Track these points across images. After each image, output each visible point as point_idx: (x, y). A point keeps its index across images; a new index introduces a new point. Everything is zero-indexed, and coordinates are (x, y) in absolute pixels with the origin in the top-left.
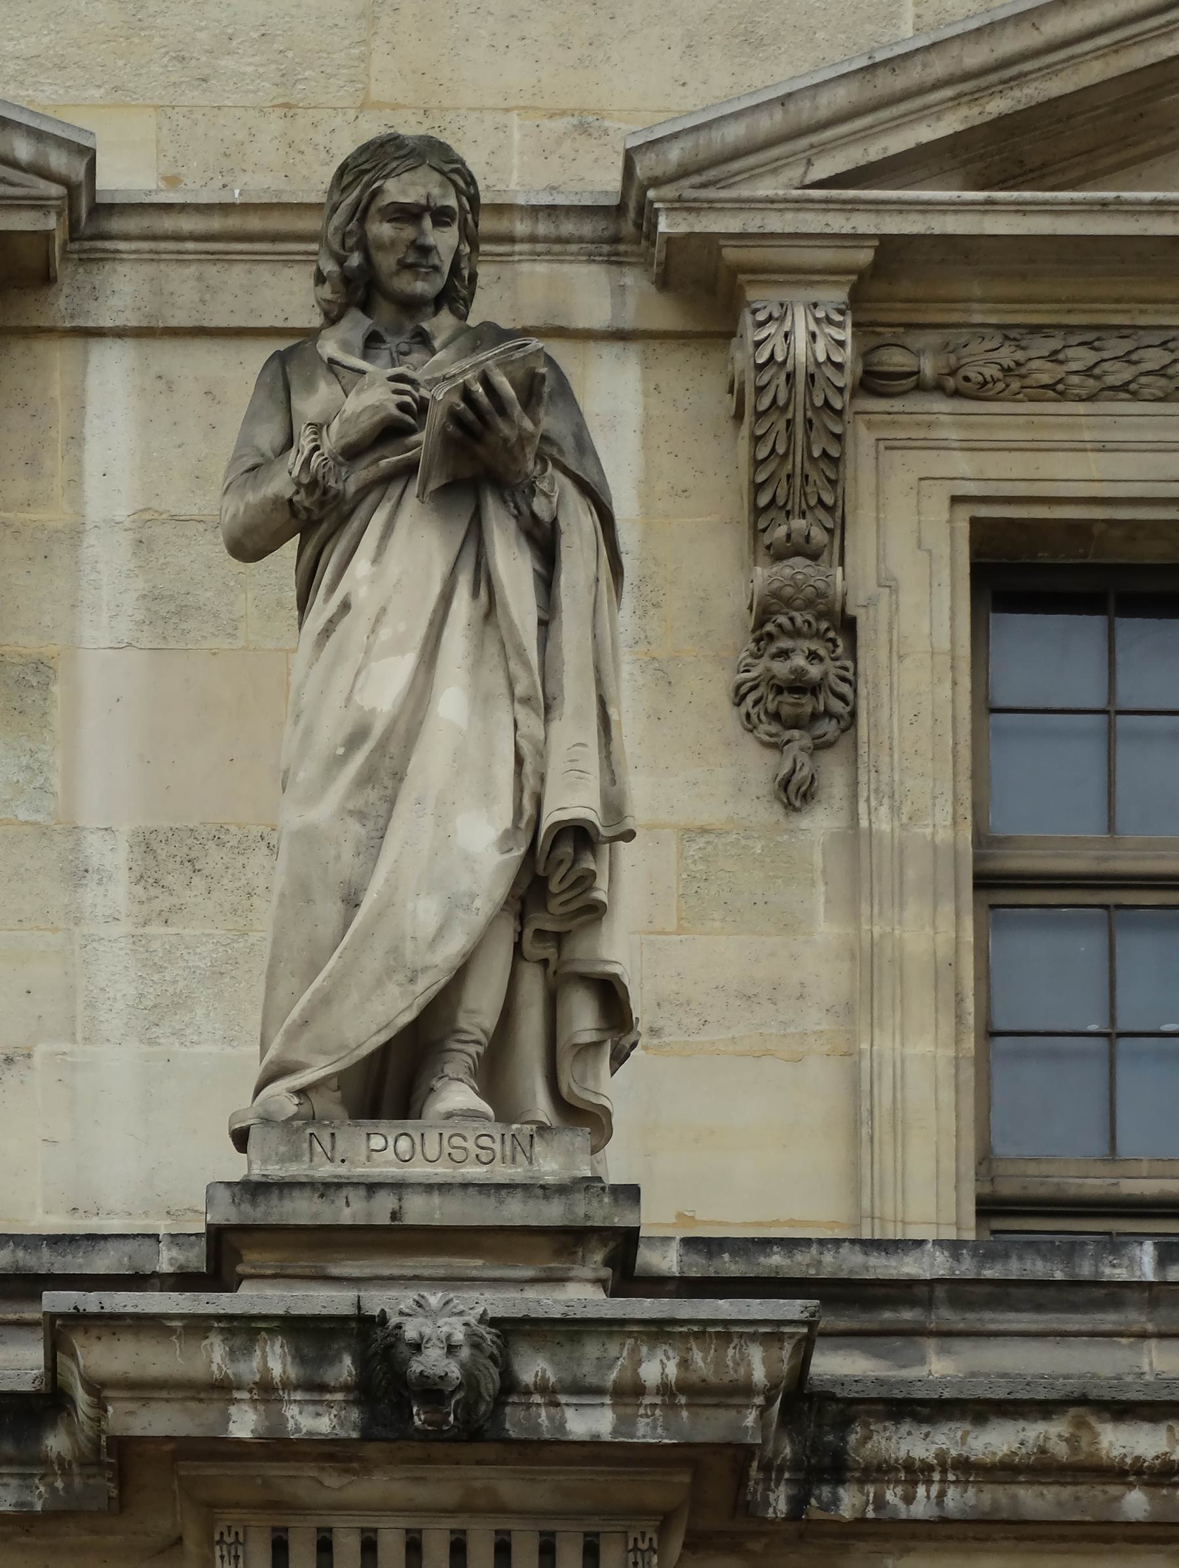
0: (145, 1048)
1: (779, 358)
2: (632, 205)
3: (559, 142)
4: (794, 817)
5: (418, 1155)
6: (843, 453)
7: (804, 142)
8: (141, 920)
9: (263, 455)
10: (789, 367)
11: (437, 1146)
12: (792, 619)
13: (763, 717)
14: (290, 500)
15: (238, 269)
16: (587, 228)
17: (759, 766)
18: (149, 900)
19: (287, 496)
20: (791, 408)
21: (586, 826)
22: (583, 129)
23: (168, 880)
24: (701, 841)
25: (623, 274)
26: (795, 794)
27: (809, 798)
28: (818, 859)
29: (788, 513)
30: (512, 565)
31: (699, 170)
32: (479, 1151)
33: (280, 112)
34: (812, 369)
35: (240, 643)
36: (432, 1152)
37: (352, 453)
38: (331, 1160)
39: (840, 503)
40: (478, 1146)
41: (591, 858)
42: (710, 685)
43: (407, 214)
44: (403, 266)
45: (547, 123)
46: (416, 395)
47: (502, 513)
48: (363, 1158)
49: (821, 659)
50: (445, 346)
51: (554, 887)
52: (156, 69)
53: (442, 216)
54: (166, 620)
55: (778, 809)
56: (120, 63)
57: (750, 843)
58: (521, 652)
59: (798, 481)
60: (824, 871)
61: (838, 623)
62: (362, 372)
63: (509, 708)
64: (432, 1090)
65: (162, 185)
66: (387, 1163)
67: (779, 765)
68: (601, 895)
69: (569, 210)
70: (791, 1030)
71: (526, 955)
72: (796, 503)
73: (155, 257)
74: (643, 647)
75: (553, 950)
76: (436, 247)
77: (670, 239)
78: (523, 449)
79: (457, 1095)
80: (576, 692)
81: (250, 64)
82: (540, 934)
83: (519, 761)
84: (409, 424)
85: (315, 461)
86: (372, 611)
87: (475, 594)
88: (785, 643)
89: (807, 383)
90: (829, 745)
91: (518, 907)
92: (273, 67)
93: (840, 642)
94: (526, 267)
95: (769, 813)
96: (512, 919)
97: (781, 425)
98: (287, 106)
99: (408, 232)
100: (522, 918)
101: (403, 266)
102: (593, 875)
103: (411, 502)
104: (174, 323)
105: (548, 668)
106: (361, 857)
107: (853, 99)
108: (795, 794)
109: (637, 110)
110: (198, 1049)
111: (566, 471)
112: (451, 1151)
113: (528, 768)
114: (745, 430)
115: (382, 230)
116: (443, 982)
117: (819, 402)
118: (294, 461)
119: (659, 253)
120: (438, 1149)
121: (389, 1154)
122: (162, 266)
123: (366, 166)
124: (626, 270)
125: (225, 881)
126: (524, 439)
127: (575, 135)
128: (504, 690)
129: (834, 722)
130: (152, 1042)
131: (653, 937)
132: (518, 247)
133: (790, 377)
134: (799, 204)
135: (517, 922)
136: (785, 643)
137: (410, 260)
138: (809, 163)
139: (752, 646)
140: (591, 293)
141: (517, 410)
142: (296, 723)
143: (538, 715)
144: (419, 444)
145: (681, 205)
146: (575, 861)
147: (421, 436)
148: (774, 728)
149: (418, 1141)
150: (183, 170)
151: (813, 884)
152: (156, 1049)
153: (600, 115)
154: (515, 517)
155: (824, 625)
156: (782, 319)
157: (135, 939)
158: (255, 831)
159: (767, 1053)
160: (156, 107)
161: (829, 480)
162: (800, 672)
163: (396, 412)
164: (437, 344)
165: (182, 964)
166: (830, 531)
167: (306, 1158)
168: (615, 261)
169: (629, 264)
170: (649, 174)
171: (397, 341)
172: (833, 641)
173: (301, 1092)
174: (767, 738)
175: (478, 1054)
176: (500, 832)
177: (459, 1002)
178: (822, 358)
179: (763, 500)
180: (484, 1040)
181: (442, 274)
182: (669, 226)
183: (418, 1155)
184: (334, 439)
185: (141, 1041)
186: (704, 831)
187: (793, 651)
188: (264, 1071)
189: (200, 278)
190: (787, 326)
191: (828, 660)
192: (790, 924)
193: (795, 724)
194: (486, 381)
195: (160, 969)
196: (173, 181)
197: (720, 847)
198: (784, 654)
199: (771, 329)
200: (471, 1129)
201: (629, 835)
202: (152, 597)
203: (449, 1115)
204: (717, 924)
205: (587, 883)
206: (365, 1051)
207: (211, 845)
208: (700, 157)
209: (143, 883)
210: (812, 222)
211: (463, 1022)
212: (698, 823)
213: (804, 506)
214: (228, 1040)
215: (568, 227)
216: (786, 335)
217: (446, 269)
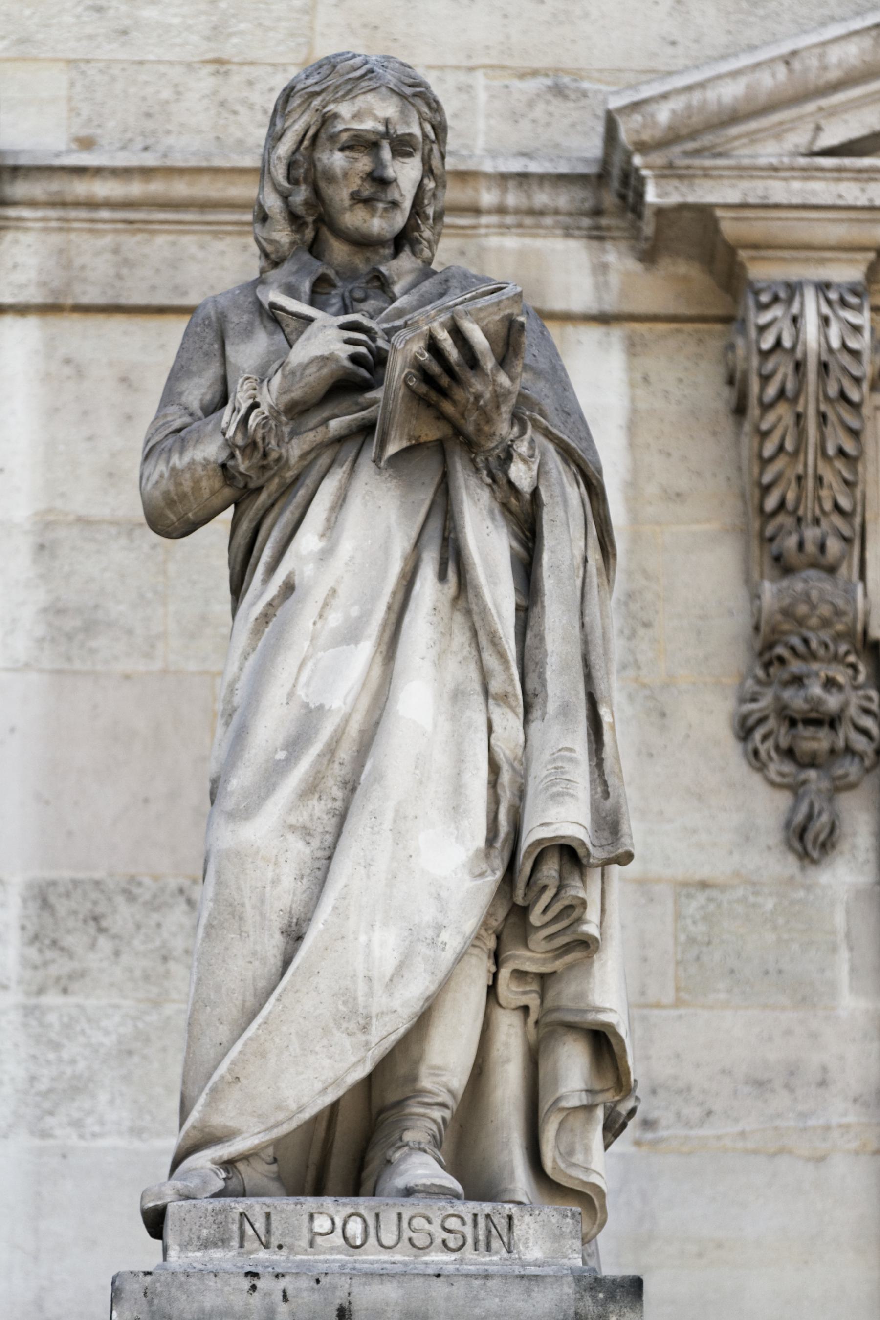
0: (37, 1142)
1: (787, 343)
2: (616, 172)
3: (531, 104)
4: (812, 871)
5: (372, 1240)
6: (862, 452)
7: (810, 107)
8: (34, 988)
9: (191, 415)
10: (799, 354)
11: (394, 1228)
12: (806, 641)
13: (773, 754)
14: (224, 466)
15: (161, 240)
16: (563, 199)
17: (768, 807)
18: (46, 964)
19: (220, 461)
20: (802, 401)
21: (574, 844)
22: (558, 91)
23: (69, 941)
24: (701, 898)
25: (604, 251)
26: (809, 841)
27: (829, 846)
28: (839, 919)
29: (799, 520)
30: (488, 543)
31: (693, 135)
32: (445, 1235)
33: (211, 68)
34: (825, 357)
35: (157, 665)
36: (388, 1238)
37: (298, 411)
38: (267, 1246)
39: (859, 509)
40: (445, 1229)
41: (579, 884)
42: (709, 716)
43: (364, 144)
44: (357, 198)
45: (518, 85)
46: (373, 345)
47: (473, 481)
48: (304, 1243)
49: (840, 687)
50: (406, 292)
51: (536, 917)
52: (68, 19)
53: (403, 147)
54: (70, 637)
55: (792, 861)
56: (27, 12)
57: (760, 900)
58: (495, 641)
59: (810, 483)
60: (848, 935)
61: (859, 645)
62: (310, 320)
63: (483, 707)
64: (389, 1162)
65: (74, 146)
66: (332, 1249)
67: (794, 810)
68: (591, 928)
69: (542, 178)
70: (812, 1122)
71: (502, 1001)
72: (808, 508)
73: (65, 225)
74: (631, 673)
75: (534, 996)
76: (395, 180)
77: (660, 212)
78: (498, 407)
79: (422, 1168)
80: (560, 684)
81: (175, 15)
82: (520, 975)
83: (494, 768)
84: (365, 380)
85: (253, 422)
86: (319, 594)
87: (442, 576)
88: (796, 666)
89: (819, 374)
90: (851, 787)
91: (491, 943)
92: (203, 18)
93: (862, 668)
94: (494, 241)
95: (782, 865)
96: (485, 957)
97: (789, 420)
98: (219, 61)
99: (364, 163)
100: (497, 957)
101: (357, 198)
102: (584, 903)
103: (366, 468)
104: (85, 300)
105: (528, 661)
106: (305, 881)
107: (867, 58)
108: (809, 841)
109: (620, 70)
110: (101, 1143)
111: (548, 434)
112: (412, 1235)
113: (506, 777)
114: (747, 427)
115: (337, 160)
116: (402, 1031)
117: (833, 391)
118: (228, 418)
119: (648, 228)
120: (396, 1233)
121: (337, 1239)
122: (73, 236)
123: (317, 88)
124: (609, 245)
125: (136, 943)
126: (499, 397)
127: (549, 97)
128: (477, 687)
129: (857, 760)
130: (45, 1134)
131: (645, 1011)
132: (484, 220)
133: (799, 366)
134: (808, 174)
135: (492, 961)
136: (796, 666)
137: (366, 193)
138: (818, 129)
139: (760, 673)
140: (569, 271)
141: (489, 363)
142: (227, 724)
143: (517, 715)
144: (374, 402)
145: (669, 172)
146: (560, 888)
147: (377, 394)
148: (788, 767)
149: (371, 1222)
150: (99, 131)
151: (834, 949)
152: (50, 1142)
153: (577, 75)
154: (489, 485)
155: (843, 648)
156: (790, 301)
157: (29, 1011)
158: (173, 883)
159: (782, 1151)
160: (69, 61)
161: (846, 482)
162: (816, 704)
163: (347, 364)
164: (397, 289)
165: (81, 1039)
166: (847, 540)
167: (235, 1243)
168: (597, 236)
169: (613, 238)
170: (635, 138)
171: (350, 287)
172: (854, 667)
173: (228, 1164)
174: (778, 779)
175: (444, 1119)
176: (471, 853)
177: (417, 1062)
178: (835, 344)
179: (771, 503)
180: (450, 1101)
181: (402, 211)
182: (659, 196)
183: (372, 1240)
184: (275, 394)
185: (32, 1133)
186: (704, 885)
187: (808, 676)
188: (184, 1139)
189: (116, 251)
190: (795, 309)
191: (848, 689)
192: (807, 996)
193: (812, 762)
194: (457, 333)
195: (56, 1046)
196: (87, 143)
197: (725, 905)
198: (798, 681)
199: (777, 311)
200: (439, 1208)
201: (626, 858)
202: (55, 610)
203: (408, 1192)
204: (722, 996)
205: (576, 914)
206: (307, 1115)
207: (120, 900)
208: (695, 119)
209: (37, 944)
210: (821, 191)
211: (426, 1082)
212: (698, 877)
213: (818, 511)
214: (136, 1132)
215: (542, 198)
216: (795, 320)
217: (407, 204)
